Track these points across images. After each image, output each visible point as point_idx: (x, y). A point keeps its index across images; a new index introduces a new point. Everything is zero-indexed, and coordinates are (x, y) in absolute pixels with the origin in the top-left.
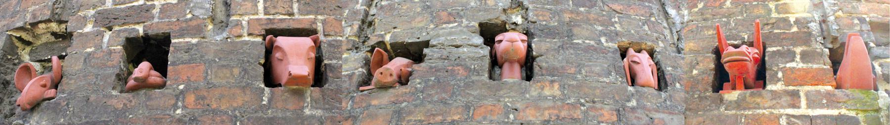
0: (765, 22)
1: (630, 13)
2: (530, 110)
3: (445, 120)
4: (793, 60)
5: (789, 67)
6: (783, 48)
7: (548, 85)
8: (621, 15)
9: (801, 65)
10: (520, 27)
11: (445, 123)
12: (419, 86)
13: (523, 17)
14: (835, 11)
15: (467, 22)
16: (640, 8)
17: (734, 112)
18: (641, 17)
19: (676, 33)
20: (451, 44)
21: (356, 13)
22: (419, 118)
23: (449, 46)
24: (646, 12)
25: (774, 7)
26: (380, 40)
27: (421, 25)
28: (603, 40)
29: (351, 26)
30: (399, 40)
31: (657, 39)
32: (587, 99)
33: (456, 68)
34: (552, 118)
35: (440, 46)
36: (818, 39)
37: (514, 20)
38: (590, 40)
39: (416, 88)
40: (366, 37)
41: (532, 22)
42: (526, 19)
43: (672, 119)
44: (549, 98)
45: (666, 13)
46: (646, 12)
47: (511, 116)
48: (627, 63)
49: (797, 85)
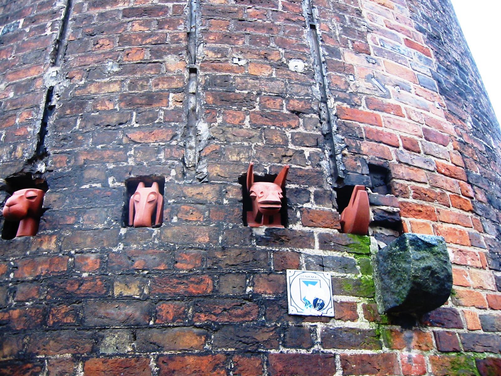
0: (284, 154)
4: (308, 201)
5: (306, 208)
6: (300, 186)
9: (315, 207)
14: (342, 150)
17: (264, 247)
25: (290, 135)
32: (77, 250)
36: (328, 180)
43: (155, 259)
49: (312, 226)
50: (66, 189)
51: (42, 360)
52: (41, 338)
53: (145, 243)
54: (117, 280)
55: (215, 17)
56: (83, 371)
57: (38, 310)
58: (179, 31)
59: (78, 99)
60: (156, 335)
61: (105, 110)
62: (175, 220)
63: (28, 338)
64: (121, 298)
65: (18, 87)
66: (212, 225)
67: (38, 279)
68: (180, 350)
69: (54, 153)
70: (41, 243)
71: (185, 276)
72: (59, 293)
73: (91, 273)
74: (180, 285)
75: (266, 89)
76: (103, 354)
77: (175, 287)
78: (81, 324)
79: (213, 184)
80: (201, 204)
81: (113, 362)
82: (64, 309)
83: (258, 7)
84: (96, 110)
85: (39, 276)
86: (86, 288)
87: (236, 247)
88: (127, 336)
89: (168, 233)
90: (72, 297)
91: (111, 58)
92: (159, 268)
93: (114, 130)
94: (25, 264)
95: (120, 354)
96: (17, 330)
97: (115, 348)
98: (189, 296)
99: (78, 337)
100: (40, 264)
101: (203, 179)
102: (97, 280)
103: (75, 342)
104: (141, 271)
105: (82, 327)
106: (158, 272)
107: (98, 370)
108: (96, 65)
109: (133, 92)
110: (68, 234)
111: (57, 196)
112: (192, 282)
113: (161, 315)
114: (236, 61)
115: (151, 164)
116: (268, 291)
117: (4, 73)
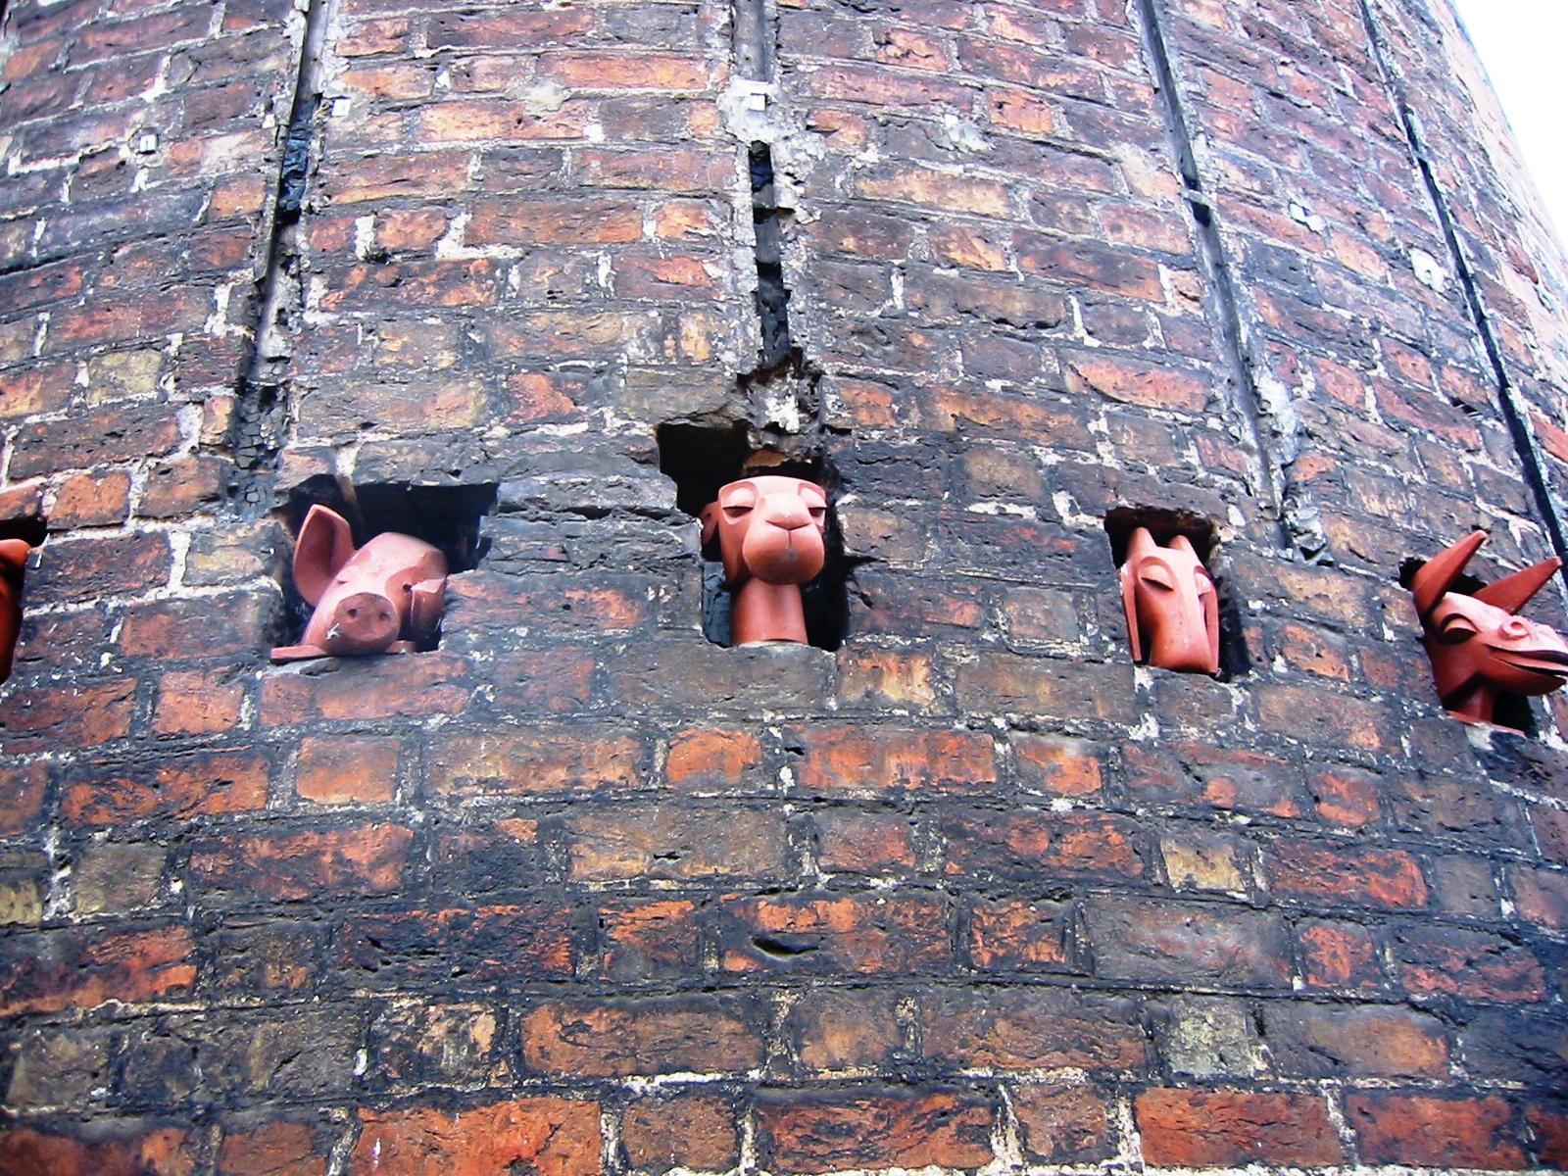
1: (1143, 401)
2: (840, 752)
3: (578, 782)
7: (893, 665)
8: (1116, 409)
10: (793, 441)
11: (580, 793)
12: (477, 655)
13: (802, 407)
15: (619, 422)
16: (1175, 379)
18: (1179, 416)
19: (1280, 470)
20: (570, 503)
21: (202, 349)
22: (493, 774)
23: (569, 510)
24: (1193, 395)
26: (321, 469)
27: (457, 421)
28: (1061, 502)
29: (201, 403)
30: (387, 473)
31: (1223, 497)
32: (1015, 718)
33: (596, 598)
34: (908, 782)
35: (533, 507)
37: (775, 417)
38: (1020, 504)
39: (469, 664)
40: (260, 447)
41: (833, 430)
42: (815, 416)
43: (1258, 780)
44: (898, 712)
45: (1254, 394)
46: (1193, 395)
47: (786, 774)
48: (1132, 581)
50: (915, 502)
51: (988, 1087)
52: (958, 1009)
53: (1221, 728)
54: (1166, 836)
55: (1213, 64)
56: (1137, 1128)
57: (924, 910)
58: (1130, 77)
59: (873, 208)
60: (1317, 1022)
61: (977, 269)
62: (1279, 665)
63: (911, 1003)
64: (1192, 895)
65: (616, 115)
66: (1374, 700)
67: (897, 800)
68: (1395, 1078)
69: (839, 374)
70: (877, 674)
71: (1349, 846)
72: (988, 860)
73: (1080, 803)
74: (1346, 874)
75: (1389, 320)
76: (1184, 1075)
77: (1335, 878)
78: (1086, 973)
79: (1347, 573)
80: (1332, 629)
81: (1222, 1104)
82: (1020, 914)
83: (1303, 68)
84: (948, 260)
85: (899, 791)
86: (1078, 851)
87: (1447, 776)
88: (1238, 1025)
89: (1276, 702)
90: (1035, 875)
91: (949, 103)
92: (1277, 811)
93: (1024, 339)
94: (832, 744)
95: (1235, 1077)
96: (863, 975)
97: (1216, 1059)
98: (1375, 911)
99: (1088, 1014)
100: (887, 748)
101: (1317, 551)
102: (1107, 828)
103: (1085, 1031)
104: (1228, 813)
105: (1092, 983)
106: (1279, 824)
107: (1183, 1129)
108: (906, 112)
109: (1050, 230)
110: (966, 661)
111: (889, 522)
112: (1373, 867)
113: (1318, 960)
114: (1299, 214)
115: (1168, 475)
116: (1547, 919)
117: (540, 50)
